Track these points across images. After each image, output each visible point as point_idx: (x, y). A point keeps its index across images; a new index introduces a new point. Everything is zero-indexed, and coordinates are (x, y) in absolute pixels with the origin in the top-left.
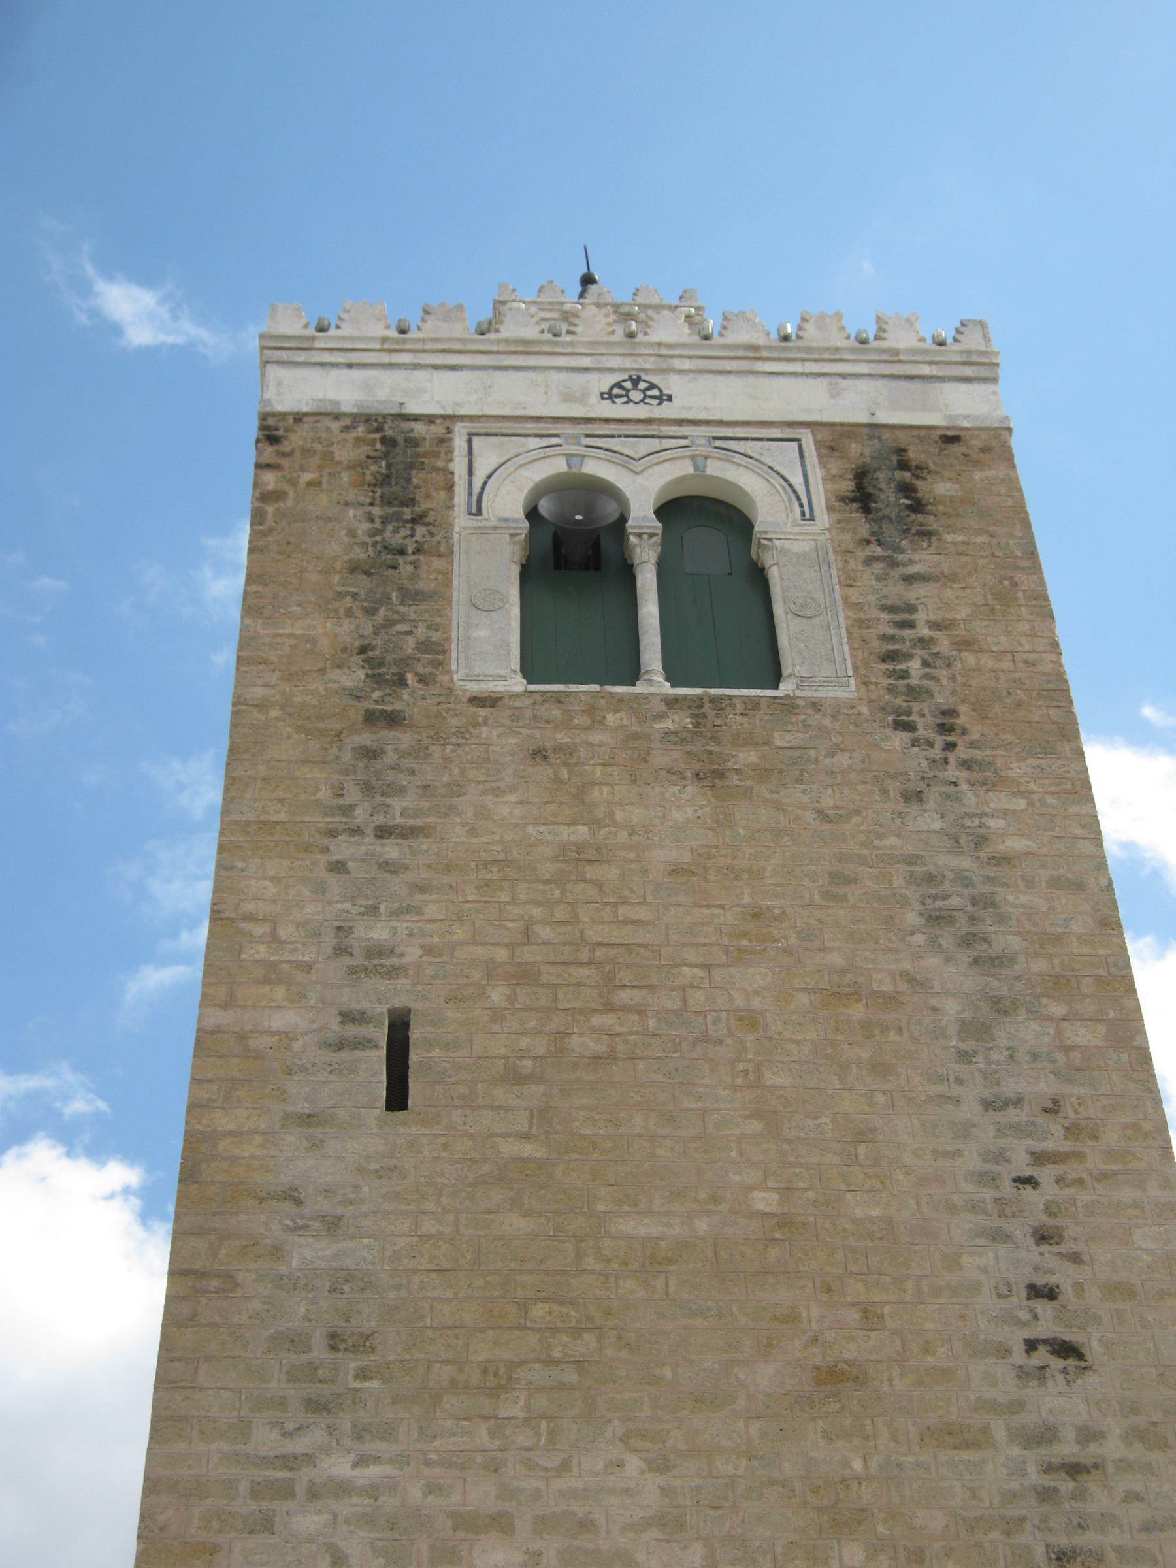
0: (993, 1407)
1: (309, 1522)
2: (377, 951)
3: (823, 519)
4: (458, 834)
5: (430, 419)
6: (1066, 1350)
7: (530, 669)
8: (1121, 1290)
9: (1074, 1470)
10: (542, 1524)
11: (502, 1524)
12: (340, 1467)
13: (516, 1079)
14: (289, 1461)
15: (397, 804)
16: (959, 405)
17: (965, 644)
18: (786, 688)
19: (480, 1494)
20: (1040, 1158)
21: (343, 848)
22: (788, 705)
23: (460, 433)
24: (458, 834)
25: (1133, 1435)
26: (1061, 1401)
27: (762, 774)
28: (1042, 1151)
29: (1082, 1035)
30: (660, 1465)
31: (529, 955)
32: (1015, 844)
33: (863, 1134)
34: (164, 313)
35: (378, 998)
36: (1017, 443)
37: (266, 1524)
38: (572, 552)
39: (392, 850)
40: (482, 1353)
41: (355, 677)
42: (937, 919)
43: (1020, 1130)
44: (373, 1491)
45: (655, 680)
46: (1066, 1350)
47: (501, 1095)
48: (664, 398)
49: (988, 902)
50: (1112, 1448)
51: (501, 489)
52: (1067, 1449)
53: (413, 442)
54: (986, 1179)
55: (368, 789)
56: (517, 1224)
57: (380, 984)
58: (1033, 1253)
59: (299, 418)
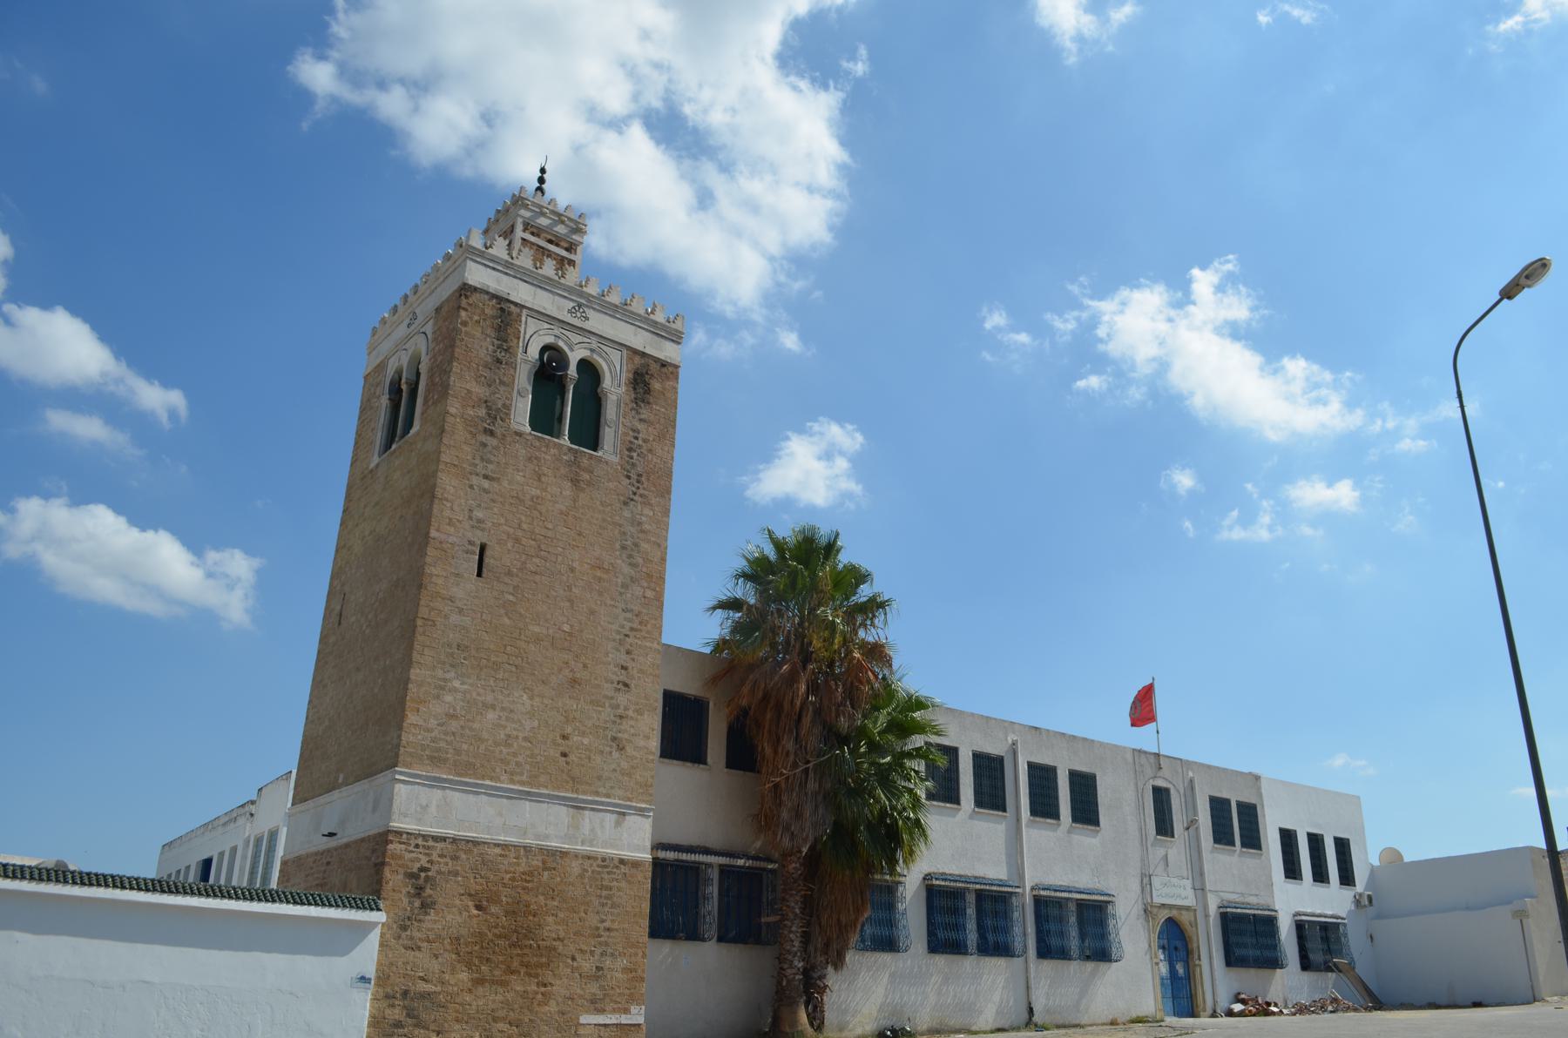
0: (606, 697)
1: (449, 698)
2: (479, 521)
3: (624, 388)
4: (505, 483)
5: (516, 304)
6: (626, 685)
7: (534, 424)
8: (641, 671)
9: (621, 717)
10: (503, 709)
11: (493, 707)
12: (457, 684)
13: (509, 573)
14: (445, 680)
15: (491, 467)
16: (667, 351)
17: (650, 451)
18: (600, 453)
19: (489, 698)
20: (632, 629)
21: (475, 480)
22: (599, 460)
23: (525, 312)
24: (505, 483)
25: (637, 711)
26: (622, 699)
27: (589, 484)
28: (652, 277)
29: (649, 594)
30: (531, 698)
31: (520, 533)
32: (647, 527)
33: (592, 612)
34: (392, 105)
35: (479, 537)
36: (681, 371)
37: (438, 697)
38: (549, 371)
39: (486, 484)
40: (493, 659)
41: (482, 412)
42: (624, 548)
43: (630, 620)
44: (465, 692)
45: (565, 441)
46: (626, 685)
47: (506, 580)
48: (587, 319)
49: (636, 545)
50: (630, 713)
51: (534, 339)
52: (620, 711)
53: (510, 313)
54: (618, 632)
55: (482, 459)
56: (507, 621)
57: (479, 533)
58: (624, 656)
59: (476, 289)
